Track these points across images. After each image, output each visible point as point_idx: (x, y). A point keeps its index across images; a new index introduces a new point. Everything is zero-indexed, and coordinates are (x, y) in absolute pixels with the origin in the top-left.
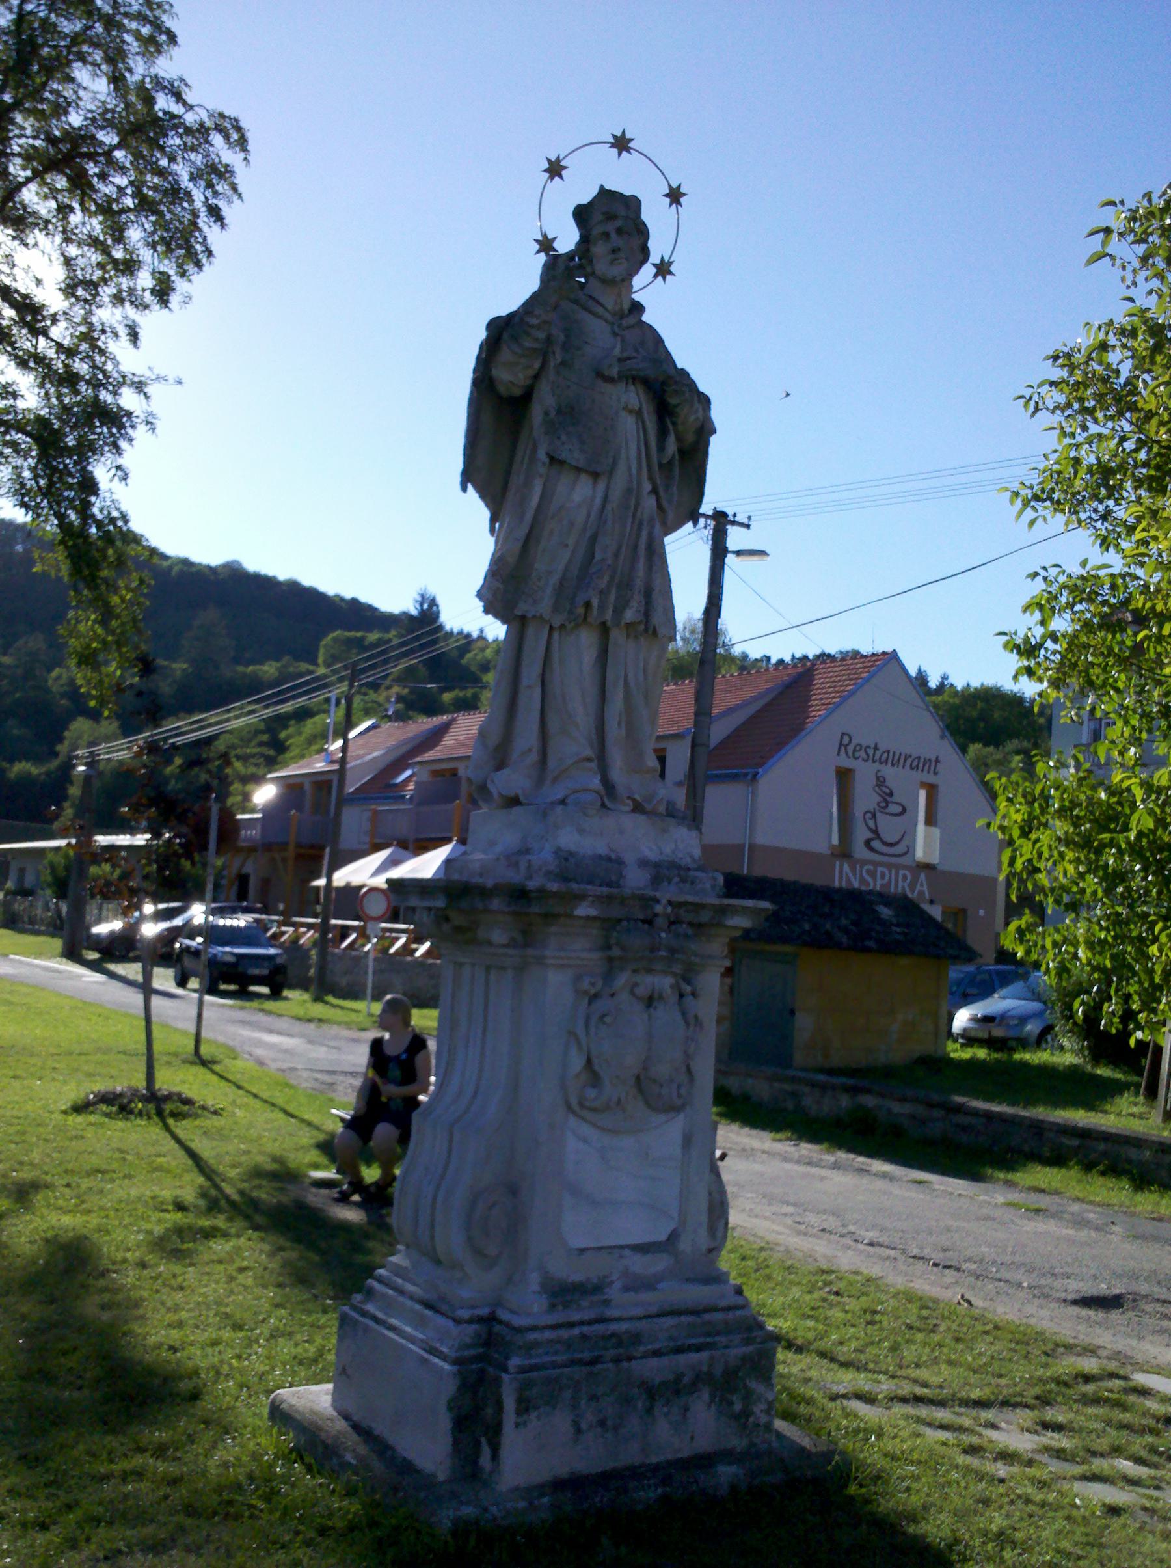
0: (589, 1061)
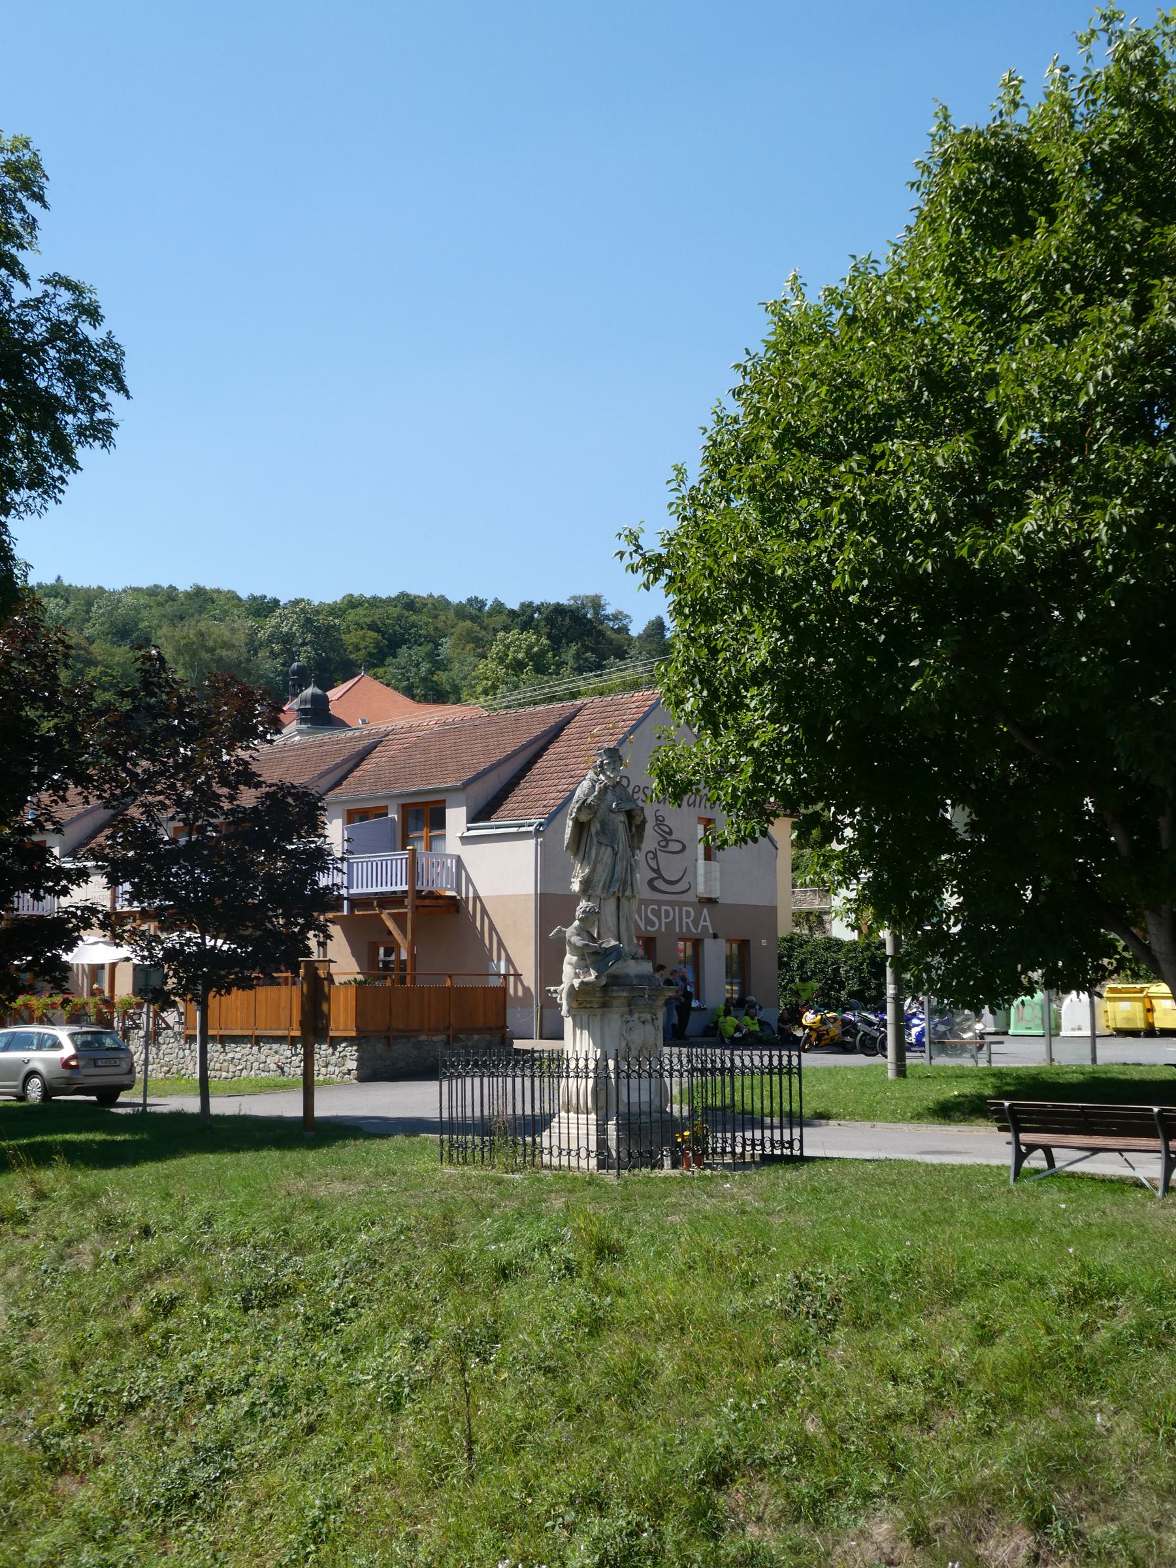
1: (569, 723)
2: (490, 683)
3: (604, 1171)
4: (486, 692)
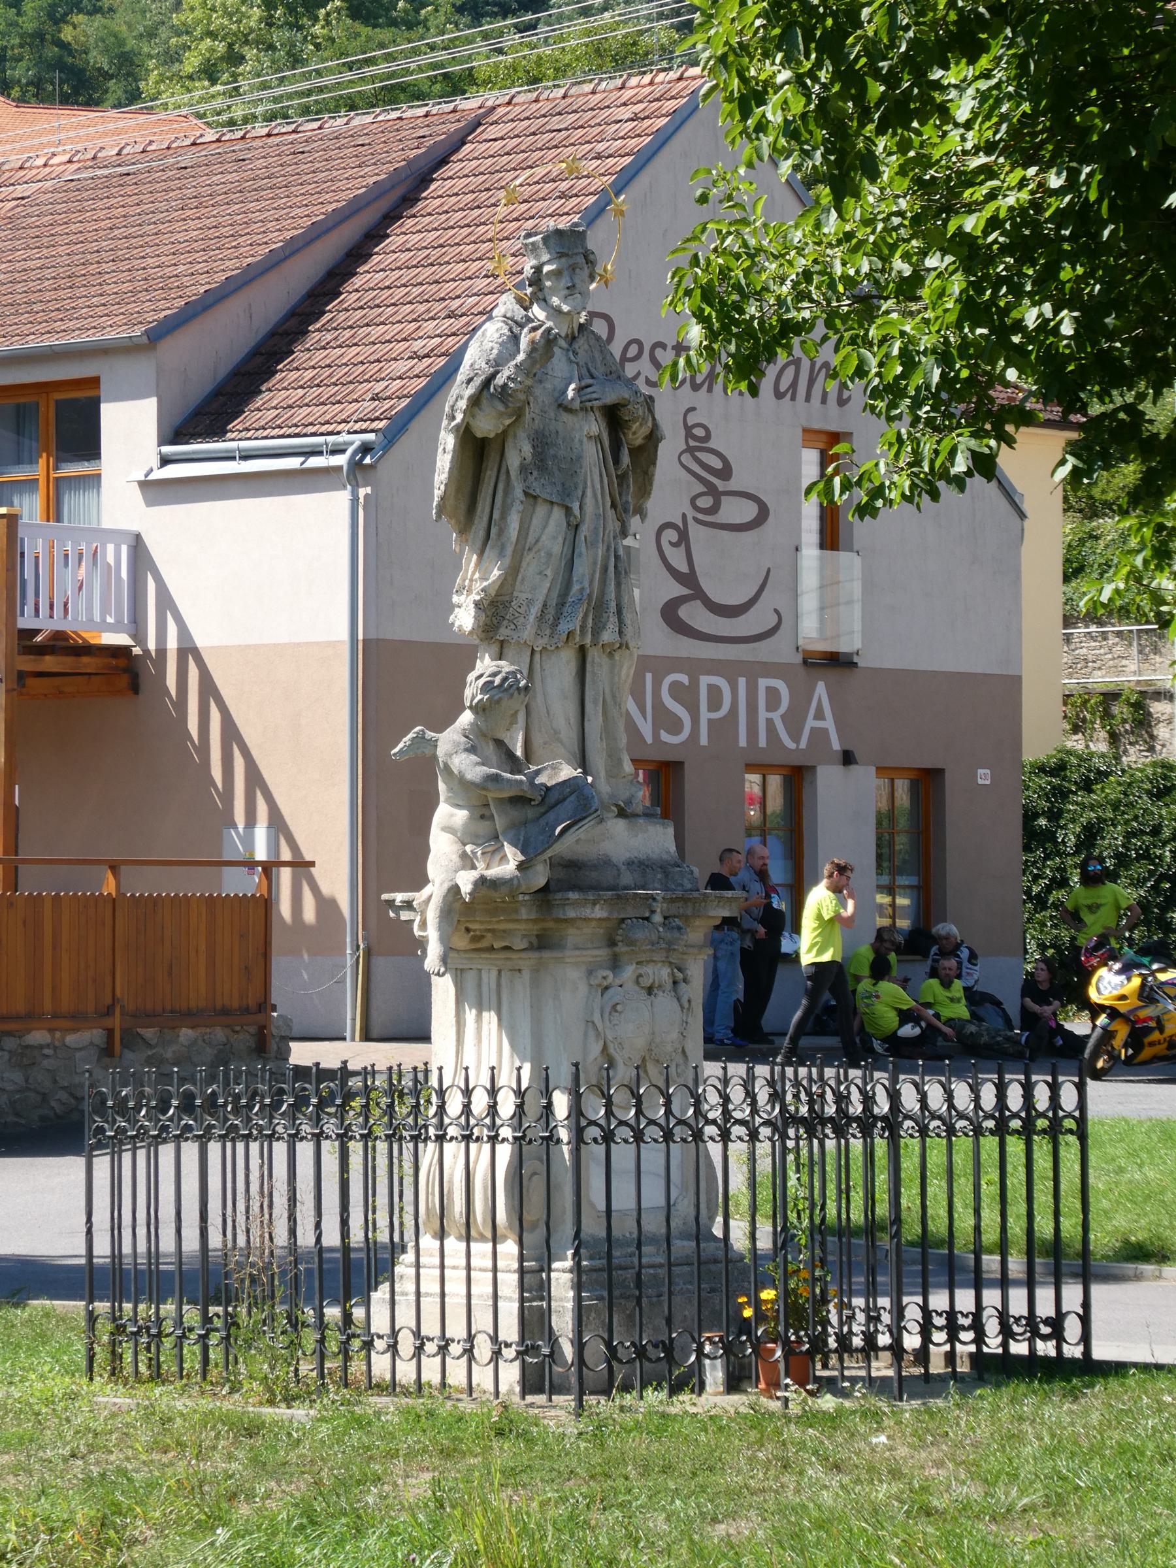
0: (605, 1048)
1: (444, 161)
2: (221, 47)
3: (541, 1399)
4: (210, 73)
